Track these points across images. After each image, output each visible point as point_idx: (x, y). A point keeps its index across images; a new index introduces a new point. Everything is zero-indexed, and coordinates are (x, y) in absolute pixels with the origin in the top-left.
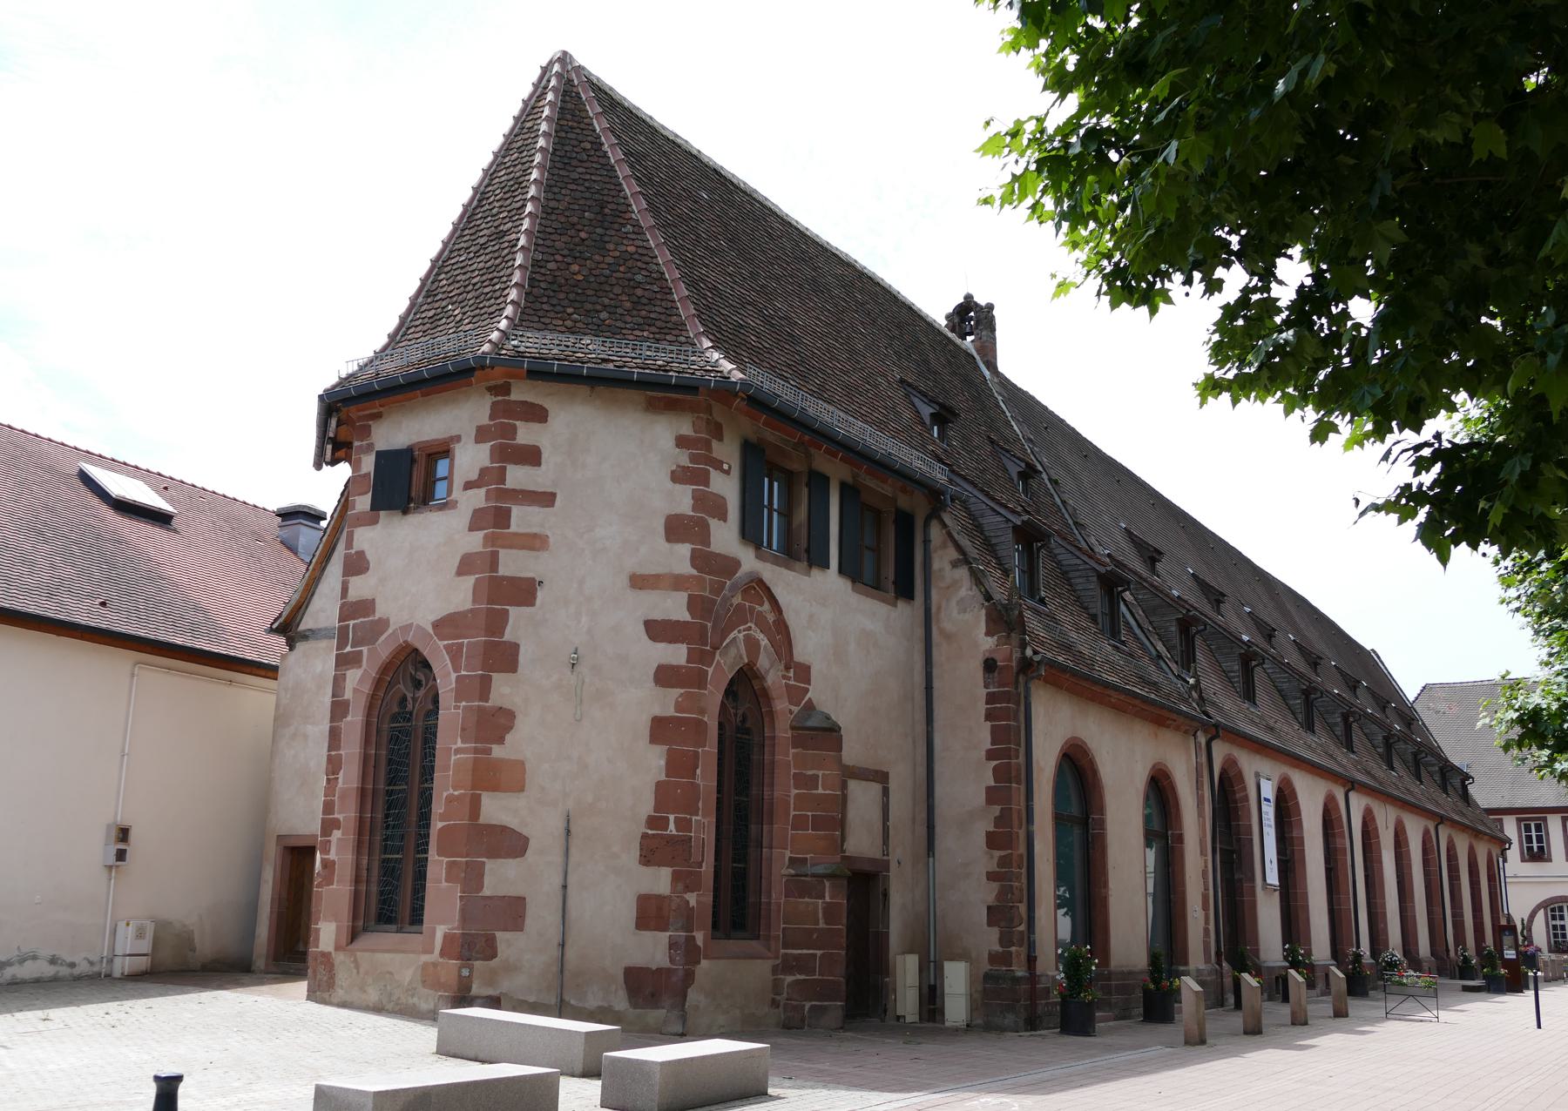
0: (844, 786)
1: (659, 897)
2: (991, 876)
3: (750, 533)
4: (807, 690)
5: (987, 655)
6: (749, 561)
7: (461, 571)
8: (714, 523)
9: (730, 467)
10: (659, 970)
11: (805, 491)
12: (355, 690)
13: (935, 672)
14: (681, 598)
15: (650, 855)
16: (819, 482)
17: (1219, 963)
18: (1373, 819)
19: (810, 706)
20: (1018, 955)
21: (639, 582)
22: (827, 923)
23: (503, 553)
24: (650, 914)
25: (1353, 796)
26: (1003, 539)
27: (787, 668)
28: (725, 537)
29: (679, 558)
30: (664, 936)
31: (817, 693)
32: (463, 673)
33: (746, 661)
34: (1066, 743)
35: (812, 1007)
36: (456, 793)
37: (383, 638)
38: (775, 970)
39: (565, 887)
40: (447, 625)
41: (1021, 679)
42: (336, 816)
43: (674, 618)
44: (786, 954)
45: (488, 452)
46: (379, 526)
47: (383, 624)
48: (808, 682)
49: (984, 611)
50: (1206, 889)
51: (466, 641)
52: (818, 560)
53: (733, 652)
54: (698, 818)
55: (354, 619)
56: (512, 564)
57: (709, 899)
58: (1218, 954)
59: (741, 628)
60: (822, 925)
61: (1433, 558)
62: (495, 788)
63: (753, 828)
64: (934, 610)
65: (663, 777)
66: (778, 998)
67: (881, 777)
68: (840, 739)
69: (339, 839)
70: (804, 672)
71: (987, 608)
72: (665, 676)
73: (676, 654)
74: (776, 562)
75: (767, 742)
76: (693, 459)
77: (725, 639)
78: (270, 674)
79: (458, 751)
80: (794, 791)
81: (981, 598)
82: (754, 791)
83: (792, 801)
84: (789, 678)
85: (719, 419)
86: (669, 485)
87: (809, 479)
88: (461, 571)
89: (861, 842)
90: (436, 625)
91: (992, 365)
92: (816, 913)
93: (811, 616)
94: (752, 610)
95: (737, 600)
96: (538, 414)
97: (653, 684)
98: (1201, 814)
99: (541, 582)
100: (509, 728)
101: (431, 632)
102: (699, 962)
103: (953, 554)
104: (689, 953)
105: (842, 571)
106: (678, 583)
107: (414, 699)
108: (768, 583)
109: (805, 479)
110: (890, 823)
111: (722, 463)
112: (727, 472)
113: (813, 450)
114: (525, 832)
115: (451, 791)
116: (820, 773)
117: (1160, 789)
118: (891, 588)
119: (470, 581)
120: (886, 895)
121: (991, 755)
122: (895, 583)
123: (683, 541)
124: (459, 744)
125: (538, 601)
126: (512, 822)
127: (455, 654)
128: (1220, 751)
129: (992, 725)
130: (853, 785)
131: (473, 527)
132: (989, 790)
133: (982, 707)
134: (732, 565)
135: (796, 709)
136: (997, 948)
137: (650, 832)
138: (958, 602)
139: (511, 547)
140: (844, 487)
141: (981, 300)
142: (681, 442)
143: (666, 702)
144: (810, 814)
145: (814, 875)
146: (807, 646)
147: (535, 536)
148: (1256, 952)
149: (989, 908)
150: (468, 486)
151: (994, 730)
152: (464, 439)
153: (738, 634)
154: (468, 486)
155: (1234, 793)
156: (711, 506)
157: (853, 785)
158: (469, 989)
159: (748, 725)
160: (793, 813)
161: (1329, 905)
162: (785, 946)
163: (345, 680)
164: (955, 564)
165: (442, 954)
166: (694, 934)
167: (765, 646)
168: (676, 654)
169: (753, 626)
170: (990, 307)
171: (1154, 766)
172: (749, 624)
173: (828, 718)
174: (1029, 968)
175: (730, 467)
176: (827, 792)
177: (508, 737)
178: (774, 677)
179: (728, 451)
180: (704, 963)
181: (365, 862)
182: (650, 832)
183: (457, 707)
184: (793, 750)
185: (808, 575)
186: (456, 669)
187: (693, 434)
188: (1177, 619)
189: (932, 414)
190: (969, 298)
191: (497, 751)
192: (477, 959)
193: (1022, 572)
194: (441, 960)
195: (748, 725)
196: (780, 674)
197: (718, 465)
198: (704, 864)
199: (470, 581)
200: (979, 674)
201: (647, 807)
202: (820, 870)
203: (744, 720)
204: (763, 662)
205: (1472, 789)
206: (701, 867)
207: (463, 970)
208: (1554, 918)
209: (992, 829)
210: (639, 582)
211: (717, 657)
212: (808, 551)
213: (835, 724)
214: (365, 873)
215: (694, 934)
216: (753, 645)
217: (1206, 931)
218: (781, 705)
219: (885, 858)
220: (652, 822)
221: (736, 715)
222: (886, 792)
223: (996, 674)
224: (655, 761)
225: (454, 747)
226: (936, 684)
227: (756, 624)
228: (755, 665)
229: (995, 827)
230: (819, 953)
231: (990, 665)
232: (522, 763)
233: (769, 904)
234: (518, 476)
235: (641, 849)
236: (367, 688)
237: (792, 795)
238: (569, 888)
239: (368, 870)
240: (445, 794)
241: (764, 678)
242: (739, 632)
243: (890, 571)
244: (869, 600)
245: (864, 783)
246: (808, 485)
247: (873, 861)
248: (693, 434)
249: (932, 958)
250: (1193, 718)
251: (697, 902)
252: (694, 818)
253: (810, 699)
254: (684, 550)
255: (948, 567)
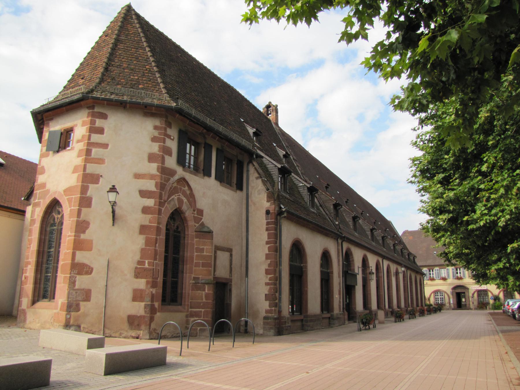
0: (215, 252)
1: (141, 290)
2: (267, 284)
3: (181, 161)
4: (201, 219)
5: (267, 209)
6: (180, 172)
7: (74, 172)
8: (167, 157)
9: (174, 138)
10: (141, 317)
11: (203, 150)
12: (38, 215)
13: (250, 215)
14: (153, 182)
15: (138, 274)
16: (208, 148)
17: (343, 311)
18: (390, 268)
19: (203, 225)
20: (275, 310)
21: (138, 176)
22: (206, 300)
23: (88, 165)
24: (137, 296)
25: (384, 261)
26: (274, 172)
27: (194, 211)
28: (171, 162)
29: (153, 168)
30: (143, 304)
31: (206, 220)
32: (72, 208)
33: (178, 206)
34: (294, 240)
35: (200, 330)
36: (68, 251)
37: (48, 196)
38: (187, 316)
39: (106, 286)
40: (68, 191)
41: (278, 217)
42: (30, 260)
43: (150, 189)
44: (191, 311)
45: (85, 129)
46: (49, 157)
47: (48, 191)
48: (202, 216)
49: (266, 194)
50: (340, 288)
51: (74, 196)
52: (207, 173)
53: (172, 203)
54: (157, 262)
55: (39, 190)
56: (92, 168)
57: (161, 291)
58: (343, 308)
59: (176, 195)
60: (204, 300)
61: (307, 26)
62: (81, 249)
63: (180, 266)
64: (250, 194)
65: (144, 247)
66: (188, 326)
67: (230, 250)
68: (212, 235)
69: (30, 268)
70: (201, 212)
71: (267, 193)
72: (145, 210)
73: (150, 202)
74: (191, 173)
75: (186, 236)
76: (160, 134)
77: (170, 197)
78: (22, 213)
79: (69, 236)
80: (196, 254)
81: (265, 190)
82: (181, 253)
83: (195, 257)
84: (195, 214)
85: (170, 121)
86: (150, 142)
87: (205, 145)
88: (74, 172)
89: (222, 272)
90: (65, 191)
91: (277, 124)
92: (202, 297)
93: (204, 193)
94: (181, 189)
95: (175, 185)
96: (104, 117)
97: (141, 213)
98: (339, 265)
99: (101, 176)
100: (87, 228)
101: (63, 193)
102: (156, 313)
103: (257, 175)
104: (152, 310)
105: (216, 178)
106: (152, 177)
107: (58, 218)
108: (187, 180)
109: (203, 146)
110: (233, 266)
111: (171, 136)
112: (173, 140)
113: (206, 136)
114: (92, 266)
115: (66, 251)
116: (205, 247)
117: (326, 256)
118: (235, 186)
119: (76, 175)
120: (230, 290)
121: (267, 243)
122: (236, 184)
123: (155, 162)
124: (70, 234)
125: (100, 182)
126: (86, 262)
127: (70, 201)
128: (345, 245)
129: (268, 233)
130: (219, 253)
131: (79, 156)
132: (267, 255)
133: (265, 227)
134: (172, 173)
135: (197, 225)
136: (268, 308)
137: (139, 266)
138: (258, 191)
139: (91, 163)
140: (218, 150)
141: (274, 103)
142: (156, 128)
143: (146, 219)
144: (201, 261)
145: (201, 283)
146: (202, 203)
147: (100, 159)
148: (355, 308)
149: (266, 295)
150: (78, 141)
151: (269, 234)
152: (78, 125)
153: (175, 197)
154: (78, 141)
155: (349, 259)
156: (167, 151)
157: (219, 253)
158: (69, 322)
159: (179, 230)
160: (195, 261)
161: (72, 256)
162: (191, 308)
163: (35, 211)
164: (257, 178)
165: (61, 310)
166: (154, 303)
167: (186, 202)
168: (150, 202)
169: (181, 194)
170: (277, 106)
171: (324, 249)
172: (179, 194)
173: (208, 228)
174: (279, 314)
175: (174, 138)
176: (207, 254)
177: (87, 231)
178: (188, 213)
179: (173, 132)
180: (158, 314)
181: (39, 276)
182: (139, 266)
183: (69, 220)
184: (196, 239)
185: (203, 178)
186: (70, 207)
187: (160, 125)
188: (333, 204)
189: (253, 132)
190: (270, 103)
191: (83, 236)
192: (72, 312)
193: (281, 184)
194: (60, 312)
195: (179, 230)
196: (191, 212)
197: (169, 137)
198: (159, 279)
199: (76, 175)
200: (264, 216)
201: (138, 257)
202: (203, 281)
203: (178, 228)
204: (184, 208)
205: (416, 260)
206: (157, 279)
207: (67, 315)
208: (443, 298)
209: (267, 268)
210: (138, 176)
211: (166, 204)
212: (203, 170)
213: (211, 230)
214: (39, 281)
215: (154, 303)
216: (180, 201)
217: (340, 302)
218: (191, 223)
219: (231, 278)
220: (139, 263)
221: (174, 226)
222: (231, 255)
223: (270, 215)
224: (140, 241)
225: (68, 235)
226: (250, 219)
227: (182, 194)
228: (181, 208)
229: (269, 267)
230: (203, 310)
231: (268, 212)
232: (92, 241)
233: (185, 293)
234: (96, 138)
235: (135, 273)
236: (41, 214)
237: (195, 255)
238: (108, 286)
239: (40, 279)
240: (64, 252)
241: (185, 213)
242: (175, 196)
243: (235, 180)
244: (226, 189)
245: (223, 252)
246: (204, 148)
247: (226, 279)
248: (160, 125)
249: (246, 312)
250: (337, 234)
251: (156, 292)
252: (155, 262)
253: (203, 222)
254: (155, 165)
255: (254, 178)
